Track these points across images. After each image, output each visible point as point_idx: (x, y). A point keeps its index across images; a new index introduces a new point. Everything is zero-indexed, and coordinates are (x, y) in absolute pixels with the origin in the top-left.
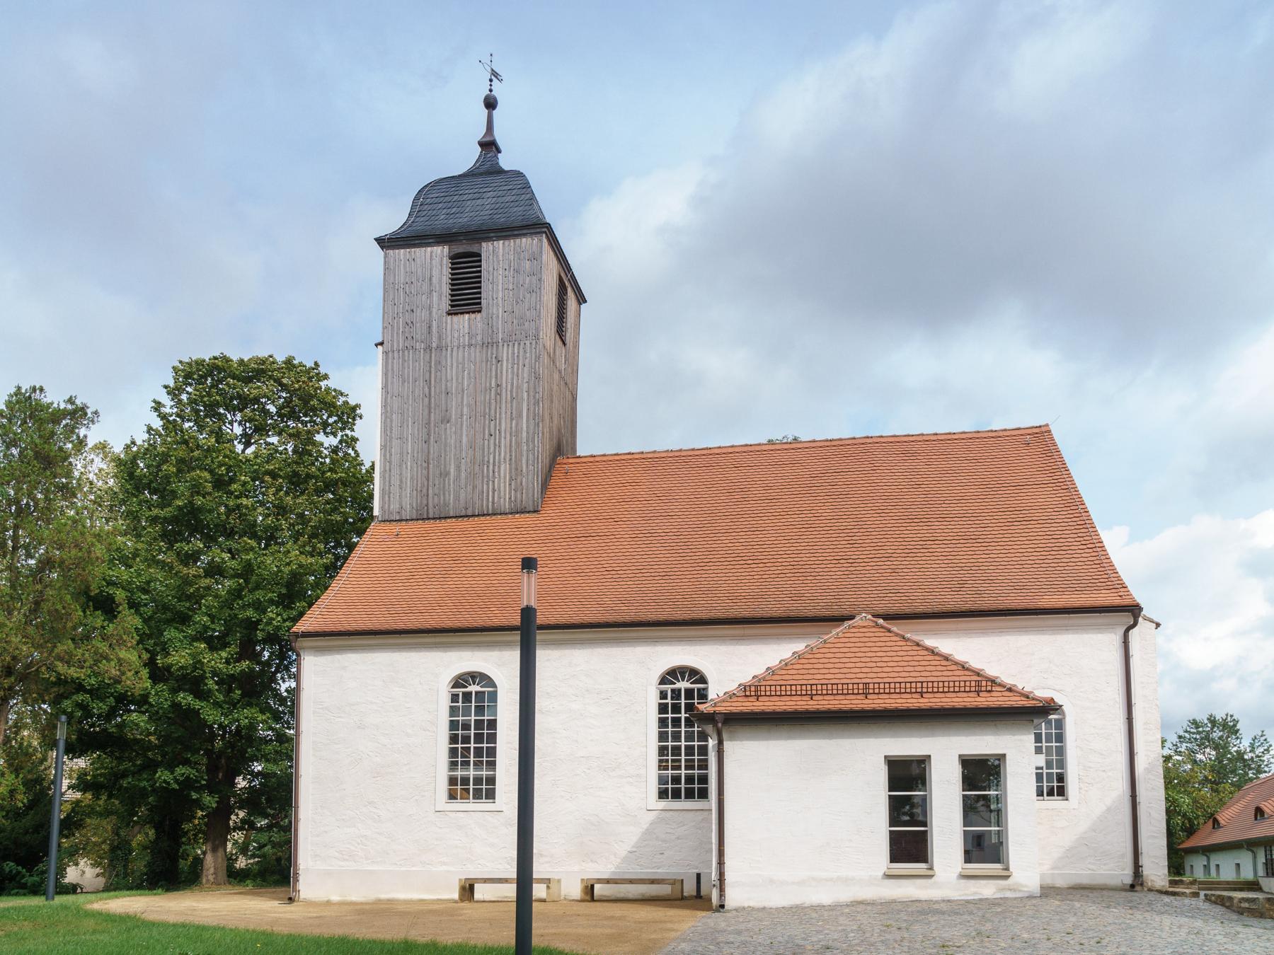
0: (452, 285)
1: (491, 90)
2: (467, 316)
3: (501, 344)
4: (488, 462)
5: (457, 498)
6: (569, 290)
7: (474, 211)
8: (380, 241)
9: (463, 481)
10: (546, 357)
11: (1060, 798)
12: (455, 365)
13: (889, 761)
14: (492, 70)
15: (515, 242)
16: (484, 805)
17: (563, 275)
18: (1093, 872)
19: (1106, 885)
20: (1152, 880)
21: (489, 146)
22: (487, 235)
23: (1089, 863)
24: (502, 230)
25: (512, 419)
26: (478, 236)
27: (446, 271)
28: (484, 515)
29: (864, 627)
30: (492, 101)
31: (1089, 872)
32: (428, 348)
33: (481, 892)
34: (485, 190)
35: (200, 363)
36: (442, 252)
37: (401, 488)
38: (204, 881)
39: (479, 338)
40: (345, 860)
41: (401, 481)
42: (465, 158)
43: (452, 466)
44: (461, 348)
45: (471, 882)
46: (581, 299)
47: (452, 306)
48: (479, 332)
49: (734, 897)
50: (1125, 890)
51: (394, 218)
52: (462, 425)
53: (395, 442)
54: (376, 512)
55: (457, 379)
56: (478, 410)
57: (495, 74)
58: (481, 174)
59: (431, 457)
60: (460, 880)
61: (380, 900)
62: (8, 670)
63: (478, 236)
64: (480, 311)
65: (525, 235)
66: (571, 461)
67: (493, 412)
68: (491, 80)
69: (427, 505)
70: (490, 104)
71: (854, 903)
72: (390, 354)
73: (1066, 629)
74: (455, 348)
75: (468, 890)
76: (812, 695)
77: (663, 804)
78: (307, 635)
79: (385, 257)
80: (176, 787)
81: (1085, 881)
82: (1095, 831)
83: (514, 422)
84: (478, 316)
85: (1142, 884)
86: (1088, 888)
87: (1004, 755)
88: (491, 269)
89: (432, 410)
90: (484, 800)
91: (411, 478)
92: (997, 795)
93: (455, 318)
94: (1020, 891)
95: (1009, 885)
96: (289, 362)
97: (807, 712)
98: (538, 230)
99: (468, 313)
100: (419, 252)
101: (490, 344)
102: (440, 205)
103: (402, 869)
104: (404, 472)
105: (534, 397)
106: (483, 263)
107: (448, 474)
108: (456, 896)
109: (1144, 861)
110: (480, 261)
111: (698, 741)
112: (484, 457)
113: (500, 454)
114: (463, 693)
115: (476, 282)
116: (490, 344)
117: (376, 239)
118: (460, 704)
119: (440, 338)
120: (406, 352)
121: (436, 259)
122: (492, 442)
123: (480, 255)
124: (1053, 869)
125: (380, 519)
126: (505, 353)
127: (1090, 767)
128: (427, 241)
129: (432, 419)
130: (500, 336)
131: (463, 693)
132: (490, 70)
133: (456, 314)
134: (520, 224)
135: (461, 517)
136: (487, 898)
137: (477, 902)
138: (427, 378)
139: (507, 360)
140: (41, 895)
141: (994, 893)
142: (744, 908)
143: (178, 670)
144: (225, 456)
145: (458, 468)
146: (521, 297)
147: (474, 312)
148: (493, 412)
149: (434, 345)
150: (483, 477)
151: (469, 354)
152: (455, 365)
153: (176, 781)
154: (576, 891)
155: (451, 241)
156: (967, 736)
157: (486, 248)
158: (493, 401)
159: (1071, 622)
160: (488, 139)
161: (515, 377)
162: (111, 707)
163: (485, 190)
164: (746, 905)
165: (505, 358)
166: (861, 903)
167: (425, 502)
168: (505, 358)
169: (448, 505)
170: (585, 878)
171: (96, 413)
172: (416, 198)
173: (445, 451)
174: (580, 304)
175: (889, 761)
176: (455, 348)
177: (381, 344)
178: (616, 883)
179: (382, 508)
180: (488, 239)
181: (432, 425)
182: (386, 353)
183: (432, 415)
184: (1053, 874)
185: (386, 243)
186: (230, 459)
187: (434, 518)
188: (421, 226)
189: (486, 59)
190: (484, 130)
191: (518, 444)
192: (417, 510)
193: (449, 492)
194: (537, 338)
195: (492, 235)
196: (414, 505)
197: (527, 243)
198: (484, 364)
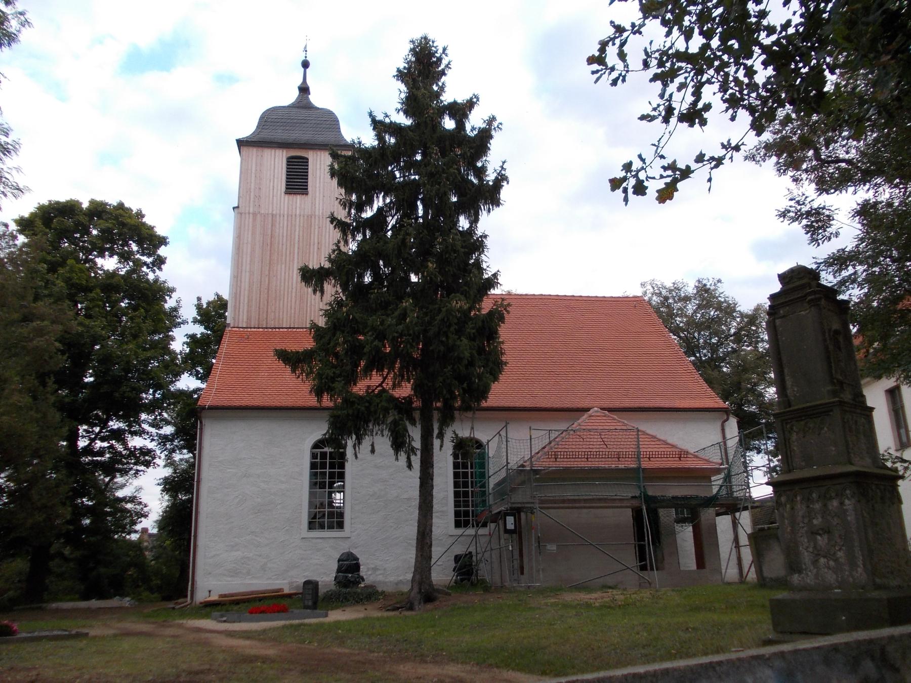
1: (306, 57)
15: (275, 152)
21: (304, 90)
40: (232, 576)
42: (289, 97)
51: (248, 129)
70: (305, 65)
77: (460, 531)
90: (335, 530)
111: (326, 469)
115: (305, 175)
125: (232, 326)
131: (321, 452)
160: (303, 86)
163: (309, 118)
188: (267, 135)
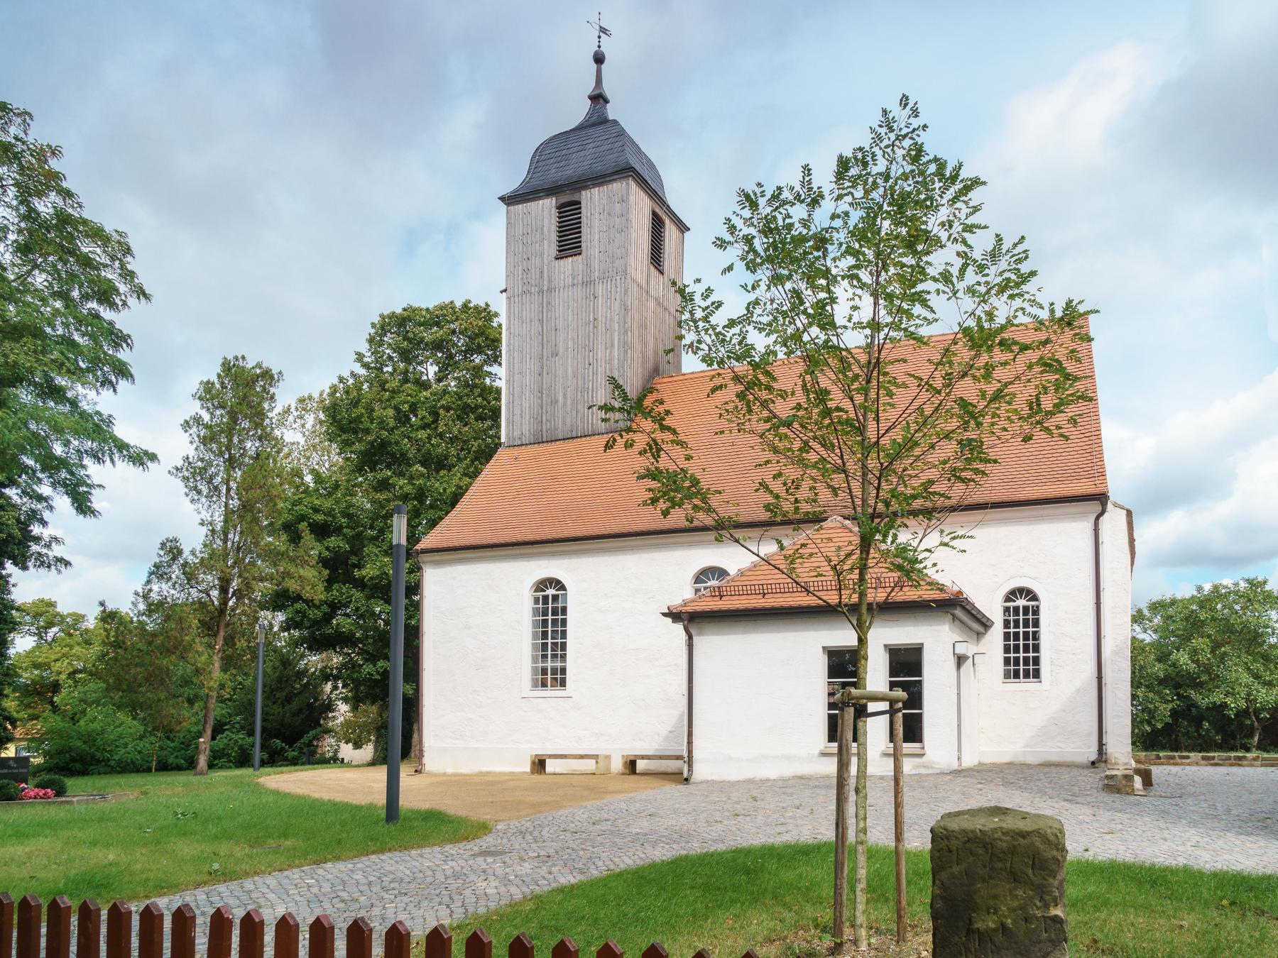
0: (560, 232)
1: (599, 47)
2: (570, 259)
3: (597, 282)
4: (588, 388)
5: (564, 423)
6: (667, 222)
7: (578, 164)
8: (502, 199)
9: (569, 407)
10: (635, 287)
11: (1035, 680)
12: (561, 303)
13: (890, 649)
14: (601, 27)
16: (559, 692)
17: (658, 210)
18: (1059, 750)
19: (1073, 762)
20: (1115, 758)
21: (598, 98)
22: (585, 184)
23: (1059, 742)
24: (596, 178)
25: (606, 349)
26: (578, 186)
27: (554, 221)
28: (585, 436)
29: (832, 528)
30: (600, 56)
31: (1059, 750)
32: (541, 292)
33: (551, 766)
34: (587, 142)
35: (392, 316)
36: (551, 203)
37: (522, 417)
38: (413, 755)
39: (580, 277)
41: (522, 412)
42: (579, 111)
43: (561, 394)
44: (566, 289)
45: (632, 758)
46: (683, 228)
47: (560, 251)
48: (580, 272)
49: (702, 771)
50: (1087, 767)
51: (514, 180)
52: (567, 357)
53: (517, 377)
54: (503, 440)
55: (564, 317)
56: (580, 343)
57: (603, 30)
58: (586, 127)
59: (545, 387)
60: (531, 756)
61: (481, 773)
62: (225, 584)
63: (578, 186)
64: (580, 254)
65: (615, 180)
66: (665, 380)
67: (591, 344)
68: (599, 37)
69: (541, 431)
70: (599, 59)
71: (78, 766)
72: (512, 299)
73: (1041, 519)
74: (562, 289)
75: (539, 764)
76: (764, 594)
79: (507, 213)
80: (378, 677)
81: (1054, 759)
82: (1064, 711)
83: (608, 351)
84: (579, 258)
85: (1106, 762)
86: (1053, 765)
87: (922, 644)
88: (589, 214)
89: (545, 346)
91: (530, 407)
93: (562, 262)
94: (933, 768)
95: (924, 762)
96: (465, 306)
97: (720, 611)
98: (626, 175)
99: (571, 256)
102: (552, 160)
104: (524, 403)
105: (624, 327)
106: (583, 210)
107: (556, 402)
108: (528, 769)
109: (1109, 740)
110: (580, 208)
112: (584, 384)
113: (597, 381)
114: (543, 596)
116: (588, 283)
117: (499, 198)
118: (541, 606)
119: (550, 281)
120: (524, 296)
121: (546, 209)
122: (591, 370)
123: (580, 203)
124: (1025, 747)
126: (600, 289)
127: (1062, 651)
128: (538, 195)
129: (545, 354)
130: (597, 274)
131: (543, 596)
132: (598, 28)
133: (561, 258)
134: (615, 169)
135: (568, 439)
136: (558, 770)
137: (549, 774)
138: (541, 318)
139: (602, 296)
140: (249, 767)
141: (911, 770)
142: (708, 781)
143: (368, 580)
144: (408, 395)
145: (565, 395)
146: (613, 237)
147: (575, 255)
148: (591, 344)
149: (545, 288)
150: (584, 402)
151: (573, 293)
152: (561, 303)
153: (378, 673)
154: (617, 765)
155: (558, 193)
156: (816, 630)
158: (591, 334)
159: (1046, 512)
160: (597, 92)
161: (609, 311)
162: (325, 614)
163: (587, 142)
164: (710, 779)
165: (600, 294)
166: (801, 778)
167: (540, 428)
168: (600, 294)
169: (556, 429)
170: (625, 754)
171: (280, 373)
172: (534, 157)
173: (555, 381)
174: (683, 232)
175: (890, 649)
176: (562, 289)
177: (505, 291)
178: (649, 759)
179: (507, 435)
180: (586, 188)
181: (545, 359)
182: (508, 298)
183: (545, 350)
184: (1024, 751)
185: (510, 200)
186: (412, 397)
187: (547, 442)
188: (536, 183)
189: (594, 19)
190: (593, 84)
192: (534, 435)
193: (558, 418)
194: (625, 272)
195: (589, 183)
196: (532, 430)
197: (617, 187)
198: (584, 301)
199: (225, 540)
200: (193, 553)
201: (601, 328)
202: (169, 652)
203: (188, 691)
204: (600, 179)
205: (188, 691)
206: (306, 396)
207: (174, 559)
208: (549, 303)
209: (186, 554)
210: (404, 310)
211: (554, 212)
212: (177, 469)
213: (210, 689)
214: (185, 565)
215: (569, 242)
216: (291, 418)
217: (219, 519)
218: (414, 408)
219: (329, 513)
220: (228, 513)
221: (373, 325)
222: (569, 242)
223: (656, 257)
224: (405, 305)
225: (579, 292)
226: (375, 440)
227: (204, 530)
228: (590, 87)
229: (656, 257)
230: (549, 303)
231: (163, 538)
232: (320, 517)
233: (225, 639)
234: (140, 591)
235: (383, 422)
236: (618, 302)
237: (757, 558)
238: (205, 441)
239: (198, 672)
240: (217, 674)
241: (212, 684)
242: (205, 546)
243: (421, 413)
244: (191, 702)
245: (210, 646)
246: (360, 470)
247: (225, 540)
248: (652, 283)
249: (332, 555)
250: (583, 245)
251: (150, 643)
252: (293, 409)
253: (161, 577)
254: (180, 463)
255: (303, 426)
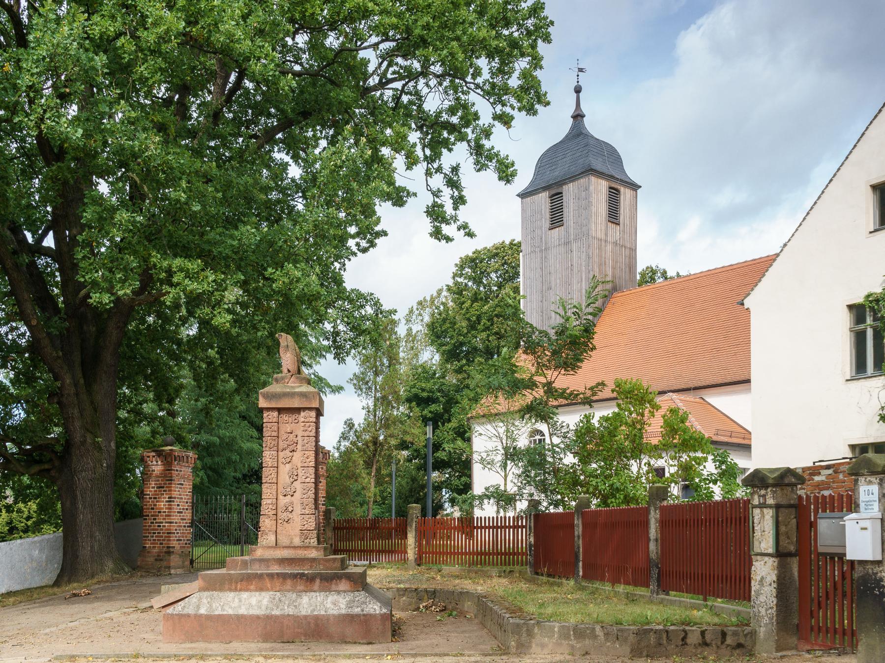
1: (578, 82)
8: (518, 195)
27: (548, 205)
32: (541, 251)
70: (578, 90)
78: (478, 417)
80: (462, 487)
92: (242, 555)
93: (553, 231)
100: (535, 197)
101: (567, 243)
103: (746, 475)
106: (564, 198)
116: (567, 243)
121: (543, 198)
123: (562, 193)
126: (574, 246)
132: (577, 70)
153: (461, 484)
157: (565, 188)
160: (576, 113)
191: (581, 296)
199: (375, 416)
200: (359, 425)
201: (575, 270)
202: (350, 478)
203: (360, 499)
204: (573, 178)
205: (360, 499)
206: (422, 299)
207: (351, 429)
208: (545, 257)
209: (356, 426)
210: (474, 253)
211: (548, 200)
212: (351, 380)
213: (369, 497)
214: (356, 431)
215: (557, 219)
216: (414, 317)
217: (371, 403)
218: (479, 318)
219: (431, 391)
220: (376, 400)
221: (456, 265)
222: (557, 219)
223: (613, 216)
224: (474, 250)
225: (562, 249)
226: (456, 342)
227: (364, 412)
228: (571, 110)
229: (613, 216)
230: (545, 257)
231: (345, 419)
232: (425, 394)
233: (376, 469)
234: (335, 446)
235: (460, 330)
236: (585, 253)
237: (707, 400)
238: (363, 363)
239: (363, 488)
240: (373, 489)
241: (370, 494)
242: (365, 420)
243: (483, 321)
244: (362, 505)
245: (369, 474)
246: (447, 361)
247: (375, 416)
248: (610, 232)
249: (433, 415)
250: (564, 219)
251: (341, 474)
252: (415, 309)
253: (345, 439)
254: (352, 377)
255: (422, 320)
